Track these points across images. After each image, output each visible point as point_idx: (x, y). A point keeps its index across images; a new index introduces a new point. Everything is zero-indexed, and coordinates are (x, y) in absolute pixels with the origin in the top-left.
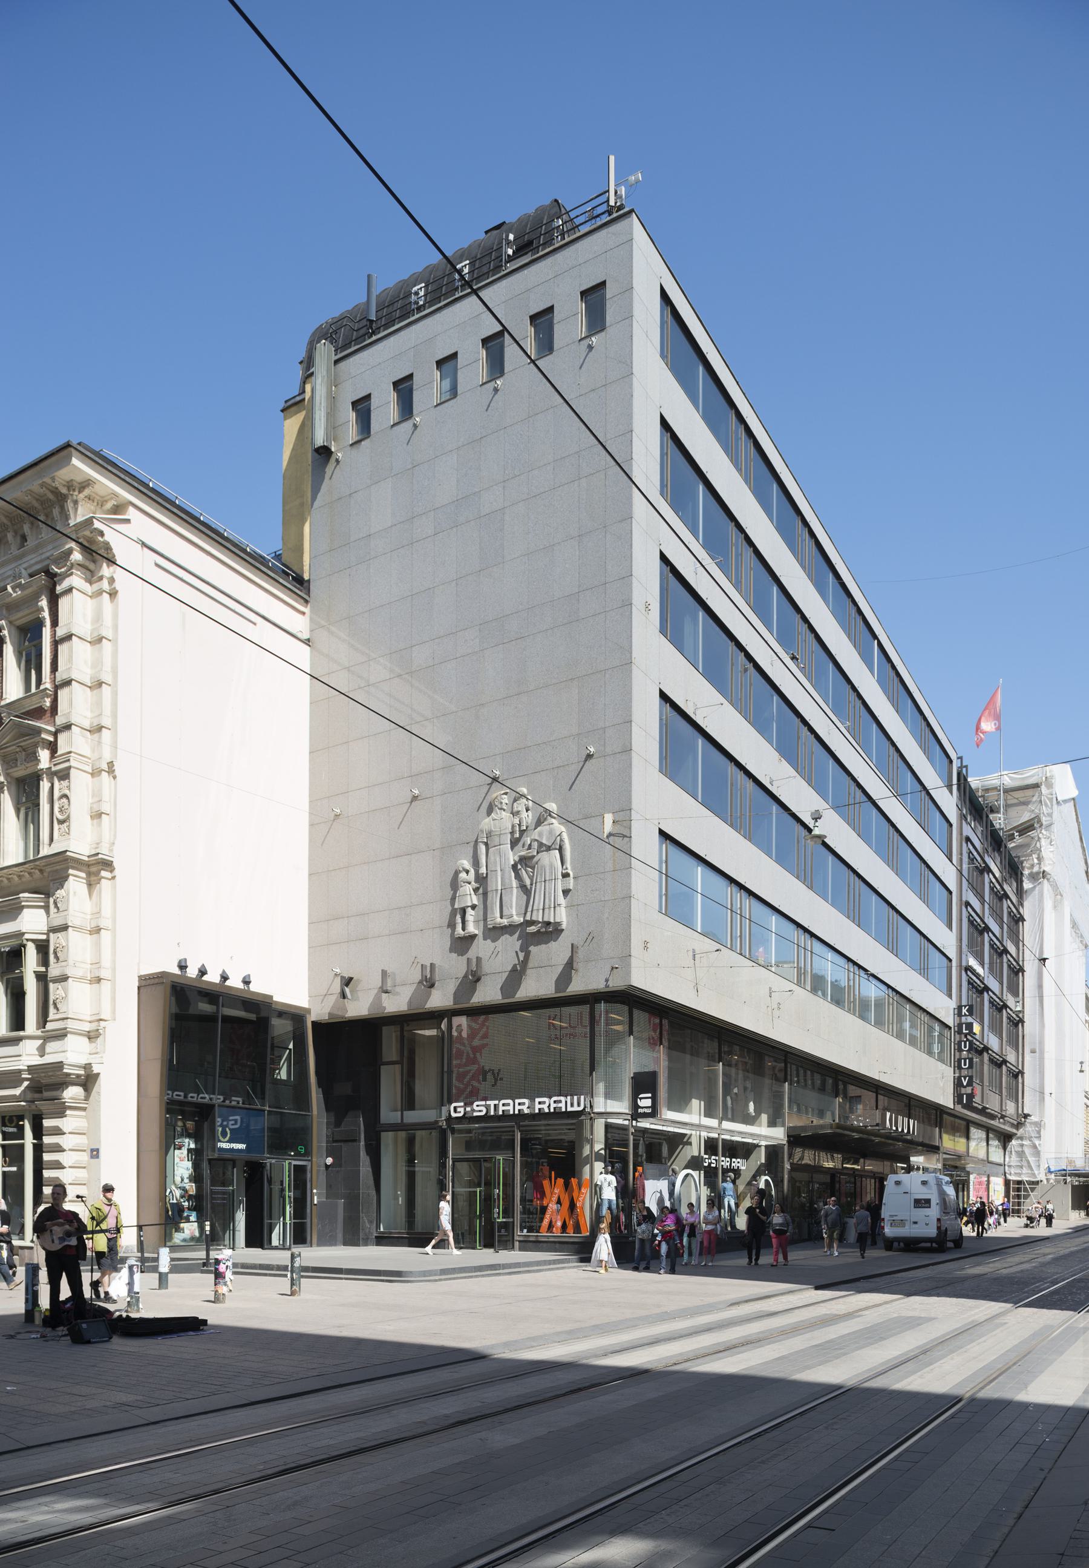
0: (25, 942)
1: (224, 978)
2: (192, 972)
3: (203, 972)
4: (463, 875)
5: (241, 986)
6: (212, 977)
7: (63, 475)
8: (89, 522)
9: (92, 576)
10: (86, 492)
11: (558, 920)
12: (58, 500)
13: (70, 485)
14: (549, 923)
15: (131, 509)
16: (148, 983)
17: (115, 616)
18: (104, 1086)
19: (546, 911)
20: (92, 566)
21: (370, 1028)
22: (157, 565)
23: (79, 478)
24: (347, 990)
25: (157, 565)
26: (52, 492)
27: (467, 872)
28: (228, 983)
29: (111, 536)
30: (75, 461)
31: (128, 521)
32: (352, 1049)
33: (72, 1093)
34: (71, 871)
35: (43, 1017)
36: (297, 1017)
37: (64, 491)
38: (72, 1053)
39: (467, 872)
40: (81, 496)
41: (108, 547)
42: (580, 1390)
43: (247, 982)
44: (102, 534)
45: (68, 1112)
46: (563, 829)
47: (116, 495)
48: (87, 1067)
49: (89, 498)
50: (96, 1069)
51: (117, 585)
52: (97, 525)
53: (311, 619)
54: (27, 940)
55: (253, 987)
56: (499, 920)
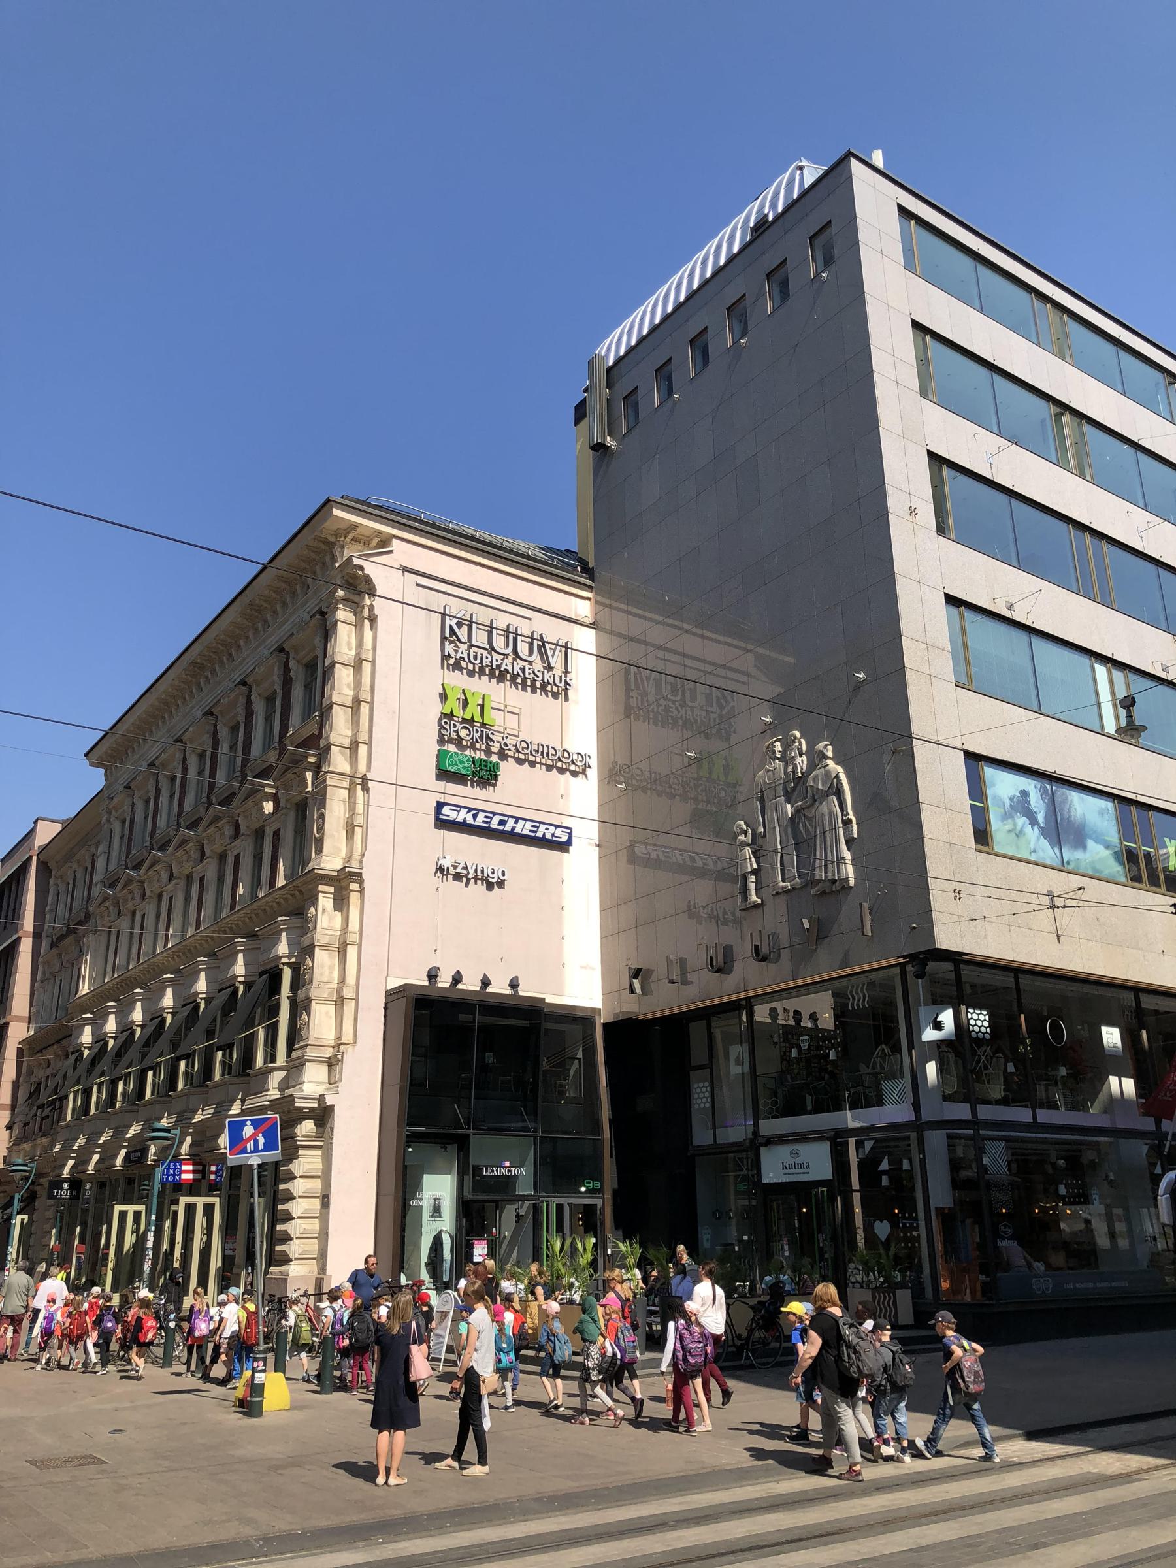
0: (281, 966)
1: (486, 983)
2: (444, 982)
3: (457, 979)
4: (742, 837)
5: (508, 991)
6: (470, 984)
7: (329, 525)
8: (350, 559)
9: (355, 606)
10: (351, 536)
11: (843, 876)
12: (327, 548)
13: (337, 534)
14: (834, 881)
15: (394, 541)
16: (393, 996)
17: (375, 639)
18: (340, 1122)
19: (830, 866)
20: (356, 598)
21: (675, 1026)
22: (418, 585)
23: (343, 526)
24: (636, 983)
25: (418, 585)
26: (324, 543)
27: (746, 833)
28: (490, 989)
29: (370, 569)
30: (336, 512)
31: (391, 552)
32: (650, 1050)
33: (306, 1128)
34: (321, 888)
35: (290, 1049)
36: (579, 1019)
37: (332, 539)
38: (313, 1082)
39: (746, 833)
40: (348, 540)
41: (368, 579)
42: (792, 1541)
43: (514, 985)
44: (361, 568)
45: (301, 1152)
46: (840, 769)
47: (379, 532)
48: (321, 1099)
49: (355, 540)
50: (329, 1100)
51: (376, 611)
52: (356, 561)
53: (597, 602)
54: (284, 964)
55: (522, 992)
56: (781, 884)
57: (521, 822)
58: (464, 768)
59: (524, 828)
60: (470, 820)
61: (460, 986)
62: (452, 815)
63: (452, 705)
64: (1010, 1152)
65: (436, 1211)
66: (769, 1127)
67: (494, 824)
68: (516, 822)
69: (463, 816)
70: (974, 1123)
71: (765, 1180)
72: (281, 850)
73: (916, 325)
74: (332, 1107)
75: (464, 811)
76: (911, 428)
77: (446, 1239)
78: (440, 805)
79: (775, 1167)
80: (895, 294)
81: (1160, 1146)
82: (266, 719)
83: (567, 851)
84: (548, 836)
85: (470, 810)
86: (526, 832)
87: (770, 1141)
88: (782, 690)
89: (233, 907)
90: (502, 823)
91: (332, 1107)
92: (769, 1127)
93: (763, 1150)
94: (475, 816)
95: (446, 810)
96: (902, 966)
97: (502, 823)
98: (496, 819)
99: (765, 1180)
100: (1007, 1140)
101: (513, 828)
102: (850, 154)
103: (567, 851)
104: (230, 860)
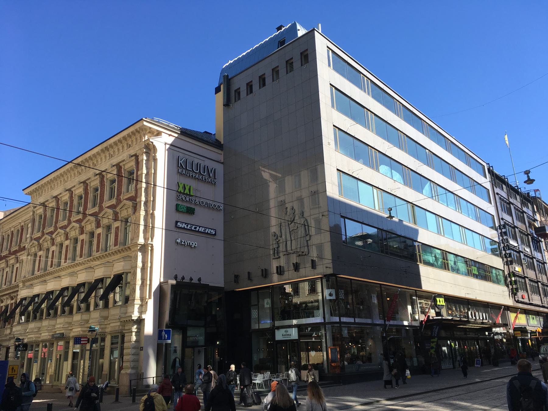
5: (198, 282)
41: (154, 146)
59: (201, 229)
60: (186, 227)
61: (184, 281)
62: (181, 226)
63: (181, 189)
64: (470, 369)
65: (175, 351)
66: (277, 323)
67: (193, 228)
69: (184, 225)
70: (340, 323)
71: (276, 339)
72: (474, 382)
73: (338, 170)
76: (330, 117)
77: (178, 360)
78: (177, 222)
79: (279, 335)
80: (327, 76)
81: (385, 328)
85: (186, 224)
87: (278, 328)
90: (195, 228)
92: (277, 323)
93: (276, 330)
94: (187, 226)
95: (179, 224)
96: (321, 278)
97: (195, 228)
98: (194, 226)
99: (276, 339)
100: (348, 327)
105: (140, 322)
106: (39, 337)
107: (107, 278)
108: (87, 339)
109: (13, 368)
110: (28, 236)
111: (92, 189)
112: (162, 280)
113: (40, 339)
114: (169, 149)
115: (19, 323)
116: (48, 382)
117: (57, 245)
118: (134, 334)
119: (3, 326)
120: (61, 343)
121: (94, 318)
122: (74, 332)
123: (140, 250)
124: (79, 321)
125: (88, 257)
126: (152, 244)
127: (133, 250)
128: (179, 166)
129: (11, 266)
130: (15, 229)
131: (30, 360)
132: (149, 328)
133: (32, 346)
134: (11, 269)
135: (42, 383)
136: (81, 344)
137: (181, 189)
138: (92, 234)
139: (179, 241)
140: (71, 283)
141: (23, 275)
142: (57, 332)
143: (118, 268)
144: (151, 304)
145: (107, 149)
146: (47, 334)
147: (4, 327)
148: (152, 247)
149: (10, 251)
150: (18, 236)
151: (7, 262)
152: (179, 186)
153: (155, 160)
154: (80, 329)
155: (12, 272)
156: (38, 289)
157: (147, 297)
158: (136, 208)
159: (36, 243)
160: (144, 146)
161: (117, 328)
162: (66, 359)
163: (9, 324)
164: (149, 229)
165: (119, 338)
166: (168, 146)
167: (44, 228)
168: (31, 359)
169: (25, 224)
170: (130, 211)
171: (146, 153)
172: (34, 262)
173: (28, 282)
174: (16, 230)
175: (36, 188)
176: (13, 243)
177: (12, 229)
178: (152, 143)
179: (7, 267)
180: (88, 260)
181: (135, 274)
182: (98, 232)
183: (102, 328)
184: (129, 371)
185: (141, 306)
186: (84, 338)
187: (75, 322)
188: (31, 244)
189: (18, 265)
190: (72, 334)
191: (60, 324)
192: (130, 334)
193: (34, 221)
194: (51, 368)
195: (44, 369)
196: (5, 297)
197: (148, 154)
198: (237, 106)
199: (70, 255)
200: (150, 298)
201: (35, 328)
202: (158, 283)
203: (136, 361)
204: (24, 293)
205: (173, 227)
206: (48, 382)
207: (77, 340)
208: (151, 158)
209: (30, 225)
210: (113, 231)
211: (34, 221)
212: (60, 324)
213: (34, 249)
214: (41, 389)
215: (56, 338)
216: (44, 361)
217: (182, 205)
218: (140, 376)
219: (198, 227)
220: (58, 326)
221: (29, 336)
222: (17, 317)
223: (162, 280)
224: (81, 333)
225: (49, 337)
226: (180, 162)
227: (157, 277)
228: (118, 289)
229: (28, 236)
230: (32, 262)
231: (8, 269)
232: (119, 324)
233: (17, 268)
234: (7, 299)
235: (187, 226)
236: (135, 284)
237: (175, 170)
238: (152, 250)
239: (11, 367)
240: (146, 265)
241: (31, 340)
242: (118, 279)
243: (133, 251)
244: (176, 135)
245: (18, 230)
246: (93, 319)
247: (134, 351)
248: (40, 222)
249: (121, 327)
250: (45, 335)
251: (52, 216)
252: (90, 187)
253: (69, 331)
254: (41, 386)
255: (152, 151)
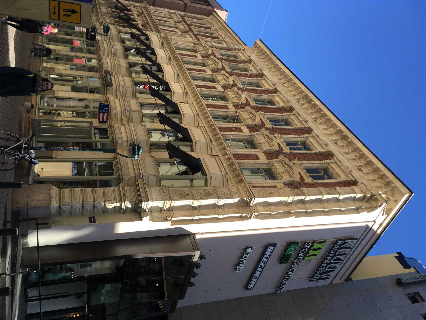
22: (55, 7)
57: (259, 273)
58: (289, 252)
59: (257, 274)
60: (265, 256)
68: (260, 271)
69: (268, 253)
74: (142, 220)
75: (270, 254)
82: (230, 55)
83: (245, 290)
84: (251, 282)
86: (255, 275)
88: (181, 303)
89: (188, 69)
90: (261, 267)
91: (142, 220)
94: (267, 258)
97: (261, 267)
101: (258, 271)
102: (251, 247)
103: (245, 290)
104: (175, 30)
105: (137, 213)
106: (104, 55)
107: (192, 146)
108: (105, 120)
109: (74, 12)
110: (214, 44)
111: (287, 117)
112: (198, 237)
113: (102, 55)
114: (367, 227)
115: (120, 32)
116: (45, 65)
117: (213, 75)
118: (118, 204)
119: (113, 15)
120: (96, 83)
121: (135, 130)
122: (114, 100)
123: (242, 200)
124: (130, 108)
125: (212, 115)
126: (250, 218)
127: (240, 188)
128: (345, 240)
129: (176, 26)
130: (213, 30)
131: (70, 42)
132: (124, 227)
133: (93, 46)
134: (173, 26)
135: (45, 58)
136: (99, 113)
137: (316, 246)
138: (235, 119)
139: (249, 250)
140: (176, 95)
141: (172, 37)
142: (112, 78)
143: (211, 165)
144: (166, 225)
145: (345, 137)
146: (109, 64)
147: (111, 17)
148: (246, 218)
149: (191, 25)
150: (207, 33)
151: (180, 22)
152: (320, 243)
153: (357, 210)
154: (119, 109)
155: (170, 27)
156: (162, 55)
157: (173, 219)
158: (294, 186)
159: (210, 52)
160: (374, 193)
161: (125, 172)
162: (74, 89)
163: (116, 22)
164: (269, 211)
165: (106, 176)
166: (370, 225)
167: (226, 60)
168: (72, 43)
169: (221, 40)
170: (286, 178)
171: (364, 197)
172: (188, 50)
173: (166, 42)
174: (212, 32)
175: (265, 52)
176: (199, 29)
177: (212, 28)
178: (380, 206)
179: (175, 22)
180: (208, 117)
181: (208, 196)
182: (242, 128)
183: (122, 144)
184: (54, 204)
185: (161, 210)
186: (108, 115)
187: (128, 102)
188: (207, 47)
189: (179, 32)
190: (111, 98)
191: (124, 82)
192: (117, 197)
193: (230, 49)
194: (62, 68)
195: (62, 59)
196: (144, 18)
197: (363, 199)
198: (401, 297)
199: (206, 91)
200: (173, 222)
201: (116, 50)
202: (193, 231)
203: (72, 212)
204: (155, 39)
205: (268, 242)
206: (45, 65)
207: (105, 108)
208: (359, 204)
209: (225, 45)
210: (251, 151)
211: (230, 49)
212: (124, 82)
213: (202, 49)
214: (35, 56)
215: (105, 77)
216: (69, 59)
217: (293, 249)
218: (43, 223)
219: (261, 270)
220: (121, 79)
221: (105, 42)
222: (129, 30)
223: (198, 237)
224: (114, 112)
225: (105, 66)
226: (350, 241)
227: (202, 230)
228: (183, 168)
229: (214, 44)
230: (187, 47)
231: (172, 22)
232: (132, 174)
233: (176, 32)
234: (143, 21)
235: (267, 258)
236: (193, 198)
237: (339, 236)
238: (242, 218)
239: (76, 8)
240: (220, 210)
241: (101, 45)
242: (194, 166)
243: (238, 189)
244: (379, 232)
245: (212, 34)
246: (135, 127)
247: (89, 207)
248: (229, 56)
249: (127, 178)
250: (107, 63)
251: (240, 69)
252: (289, 115)
253: (114, 92)
254: (41, 56)
255: (367, 205)
